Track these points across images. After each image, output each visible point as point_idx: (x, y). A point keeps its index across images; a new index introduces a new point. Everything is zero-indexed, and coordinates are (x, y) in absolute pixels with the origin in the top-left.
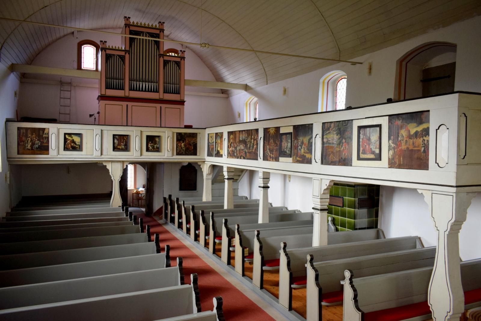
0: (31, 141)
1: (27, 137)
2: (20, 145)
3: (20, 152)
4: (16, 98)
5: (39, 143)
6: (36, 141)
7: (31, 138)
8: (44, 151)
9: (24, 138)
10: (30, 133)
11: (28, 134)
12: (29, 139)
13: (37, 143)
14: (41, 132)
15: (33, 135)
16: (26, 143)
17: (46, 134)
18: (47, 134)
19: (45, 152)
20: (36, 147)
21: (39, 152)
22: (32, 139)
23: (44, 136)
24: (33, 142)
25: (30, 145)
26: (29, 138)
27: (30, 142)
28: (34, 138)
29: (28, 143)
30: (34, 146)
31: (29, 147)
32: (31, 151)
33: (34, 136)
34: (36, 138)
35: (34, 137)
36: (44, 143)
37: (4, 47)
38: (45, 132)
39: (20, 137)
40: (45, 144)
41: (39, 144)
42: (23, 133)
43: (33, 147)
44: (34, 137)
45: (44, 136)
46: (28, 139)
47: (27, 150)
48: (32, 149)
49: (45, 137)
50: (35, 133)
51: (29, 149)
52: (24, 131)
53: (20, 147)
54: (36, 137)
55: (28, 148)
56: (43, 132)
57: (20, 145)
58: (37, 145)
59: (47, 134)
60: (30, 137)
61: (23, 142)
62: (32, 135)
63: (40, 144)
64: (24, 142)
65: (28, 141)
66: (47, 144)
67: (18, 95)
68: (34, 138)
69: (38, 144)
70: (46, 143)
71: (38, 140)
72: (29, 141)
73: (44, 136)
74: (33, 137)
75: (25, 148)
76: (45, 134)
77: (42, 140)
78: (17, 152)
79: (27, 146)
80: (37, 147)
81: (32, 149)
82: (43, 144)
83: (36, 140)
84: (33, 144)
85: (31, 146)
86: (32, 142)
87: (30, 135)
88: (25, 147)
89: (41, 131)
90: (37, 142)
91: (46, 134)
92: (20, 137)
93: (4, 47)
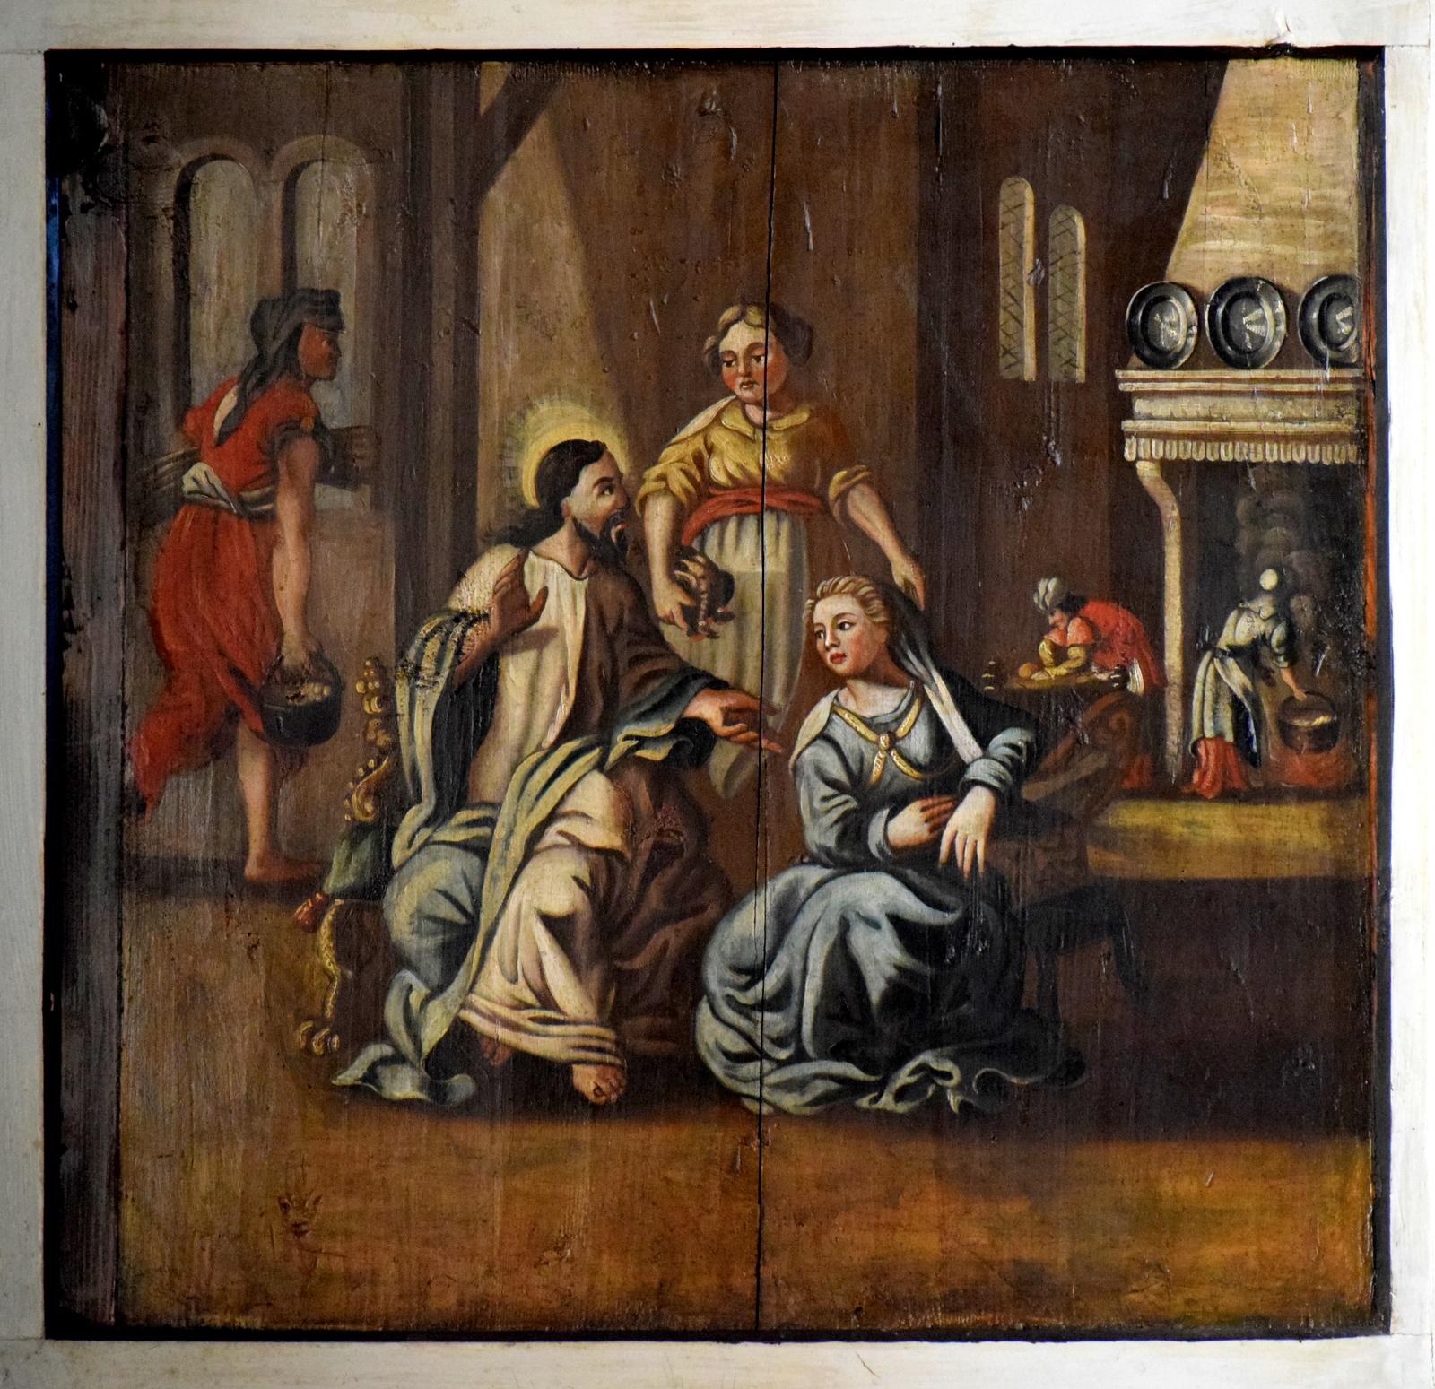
0: (628, 667)
1: (429, 486)
2: (164, 881)
3: (176, 1200)
4: (82, 224)
5: (943, 778)
6: (818, 677)
7: (611, 555)
8: (1188, 1176)
9: (312, 571)
10: (567, 284)
11: (502, 356)
12: (519, 613)
13: (866, 797)
14: (1040, 249)
15: (705, 381)
16: (392, 797)
17: (1264, 323)
18: (1309, 341)
19: (1222, 1194)
20: (808, 959)
21: (936, 1228)
22: (666, 599)
23: (1168, 415)
24: (695, 738)
25: (554, 886)
26: (527, 533)
27: (588, 722)
28: (752, 554)
29: (494, 769)
30: (748, 923)
31: (527, 983)
32: (591, 1174)
33: (730, 442)
34: (827, 550)
35: (752, 498)
36: (1166, 789)
37: (538, 667)
38: (1217, 241)
39: (143, 507)
40: (1214, 835)
41: (970, 819)
42: (291, 318)
43: (687, 981)
44: (752, 498)
45: (1144, 457)
46: (479, 587)
47: (436, 1100)
48: (664, 1076)
49: (1209, 483)
50: (778, 321)
51: (536, 1087)
52: (336, 230)
53: (139, 959)
54: (802, 502)
55: (492, 996)
56: (1136, 256)
57: (164, 881)
58: (852, 854)
59: (1309, 341)
60: (586, 499)
61: (303, 732)
62: (663, 388)
63: (1010, 817)
64: (319, 724)
65: (471, 704)
66: (1294, 835)
67: (793, 694)
68: (752, 554)
69: (908, 825)
70: (1246, 778)
71: (915, 634)
72: (535, 693)
73: (1168, 415)
74: (703, 502)
75: (362, 1023)
76: (1222, 346)
77: (1060, 651)
78: (38, 1133)
79: (460, 938)
80: (880, 956)
81: (664, 1076)
82: (1139, 816)
83: (840, 613)
84: (696, 842)
85: (600, 932)
86: (648, 734)
87: (558, 423)
88: (369, 953)
89: (1020, 202)
90: (866, 722)
91: (1264, 323)
92: (143, 507)
93: (538, 667)
